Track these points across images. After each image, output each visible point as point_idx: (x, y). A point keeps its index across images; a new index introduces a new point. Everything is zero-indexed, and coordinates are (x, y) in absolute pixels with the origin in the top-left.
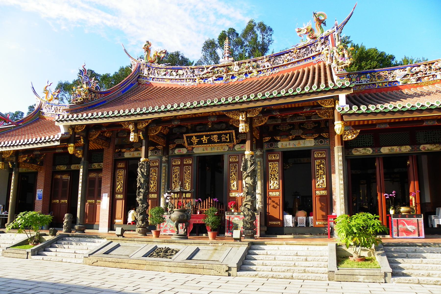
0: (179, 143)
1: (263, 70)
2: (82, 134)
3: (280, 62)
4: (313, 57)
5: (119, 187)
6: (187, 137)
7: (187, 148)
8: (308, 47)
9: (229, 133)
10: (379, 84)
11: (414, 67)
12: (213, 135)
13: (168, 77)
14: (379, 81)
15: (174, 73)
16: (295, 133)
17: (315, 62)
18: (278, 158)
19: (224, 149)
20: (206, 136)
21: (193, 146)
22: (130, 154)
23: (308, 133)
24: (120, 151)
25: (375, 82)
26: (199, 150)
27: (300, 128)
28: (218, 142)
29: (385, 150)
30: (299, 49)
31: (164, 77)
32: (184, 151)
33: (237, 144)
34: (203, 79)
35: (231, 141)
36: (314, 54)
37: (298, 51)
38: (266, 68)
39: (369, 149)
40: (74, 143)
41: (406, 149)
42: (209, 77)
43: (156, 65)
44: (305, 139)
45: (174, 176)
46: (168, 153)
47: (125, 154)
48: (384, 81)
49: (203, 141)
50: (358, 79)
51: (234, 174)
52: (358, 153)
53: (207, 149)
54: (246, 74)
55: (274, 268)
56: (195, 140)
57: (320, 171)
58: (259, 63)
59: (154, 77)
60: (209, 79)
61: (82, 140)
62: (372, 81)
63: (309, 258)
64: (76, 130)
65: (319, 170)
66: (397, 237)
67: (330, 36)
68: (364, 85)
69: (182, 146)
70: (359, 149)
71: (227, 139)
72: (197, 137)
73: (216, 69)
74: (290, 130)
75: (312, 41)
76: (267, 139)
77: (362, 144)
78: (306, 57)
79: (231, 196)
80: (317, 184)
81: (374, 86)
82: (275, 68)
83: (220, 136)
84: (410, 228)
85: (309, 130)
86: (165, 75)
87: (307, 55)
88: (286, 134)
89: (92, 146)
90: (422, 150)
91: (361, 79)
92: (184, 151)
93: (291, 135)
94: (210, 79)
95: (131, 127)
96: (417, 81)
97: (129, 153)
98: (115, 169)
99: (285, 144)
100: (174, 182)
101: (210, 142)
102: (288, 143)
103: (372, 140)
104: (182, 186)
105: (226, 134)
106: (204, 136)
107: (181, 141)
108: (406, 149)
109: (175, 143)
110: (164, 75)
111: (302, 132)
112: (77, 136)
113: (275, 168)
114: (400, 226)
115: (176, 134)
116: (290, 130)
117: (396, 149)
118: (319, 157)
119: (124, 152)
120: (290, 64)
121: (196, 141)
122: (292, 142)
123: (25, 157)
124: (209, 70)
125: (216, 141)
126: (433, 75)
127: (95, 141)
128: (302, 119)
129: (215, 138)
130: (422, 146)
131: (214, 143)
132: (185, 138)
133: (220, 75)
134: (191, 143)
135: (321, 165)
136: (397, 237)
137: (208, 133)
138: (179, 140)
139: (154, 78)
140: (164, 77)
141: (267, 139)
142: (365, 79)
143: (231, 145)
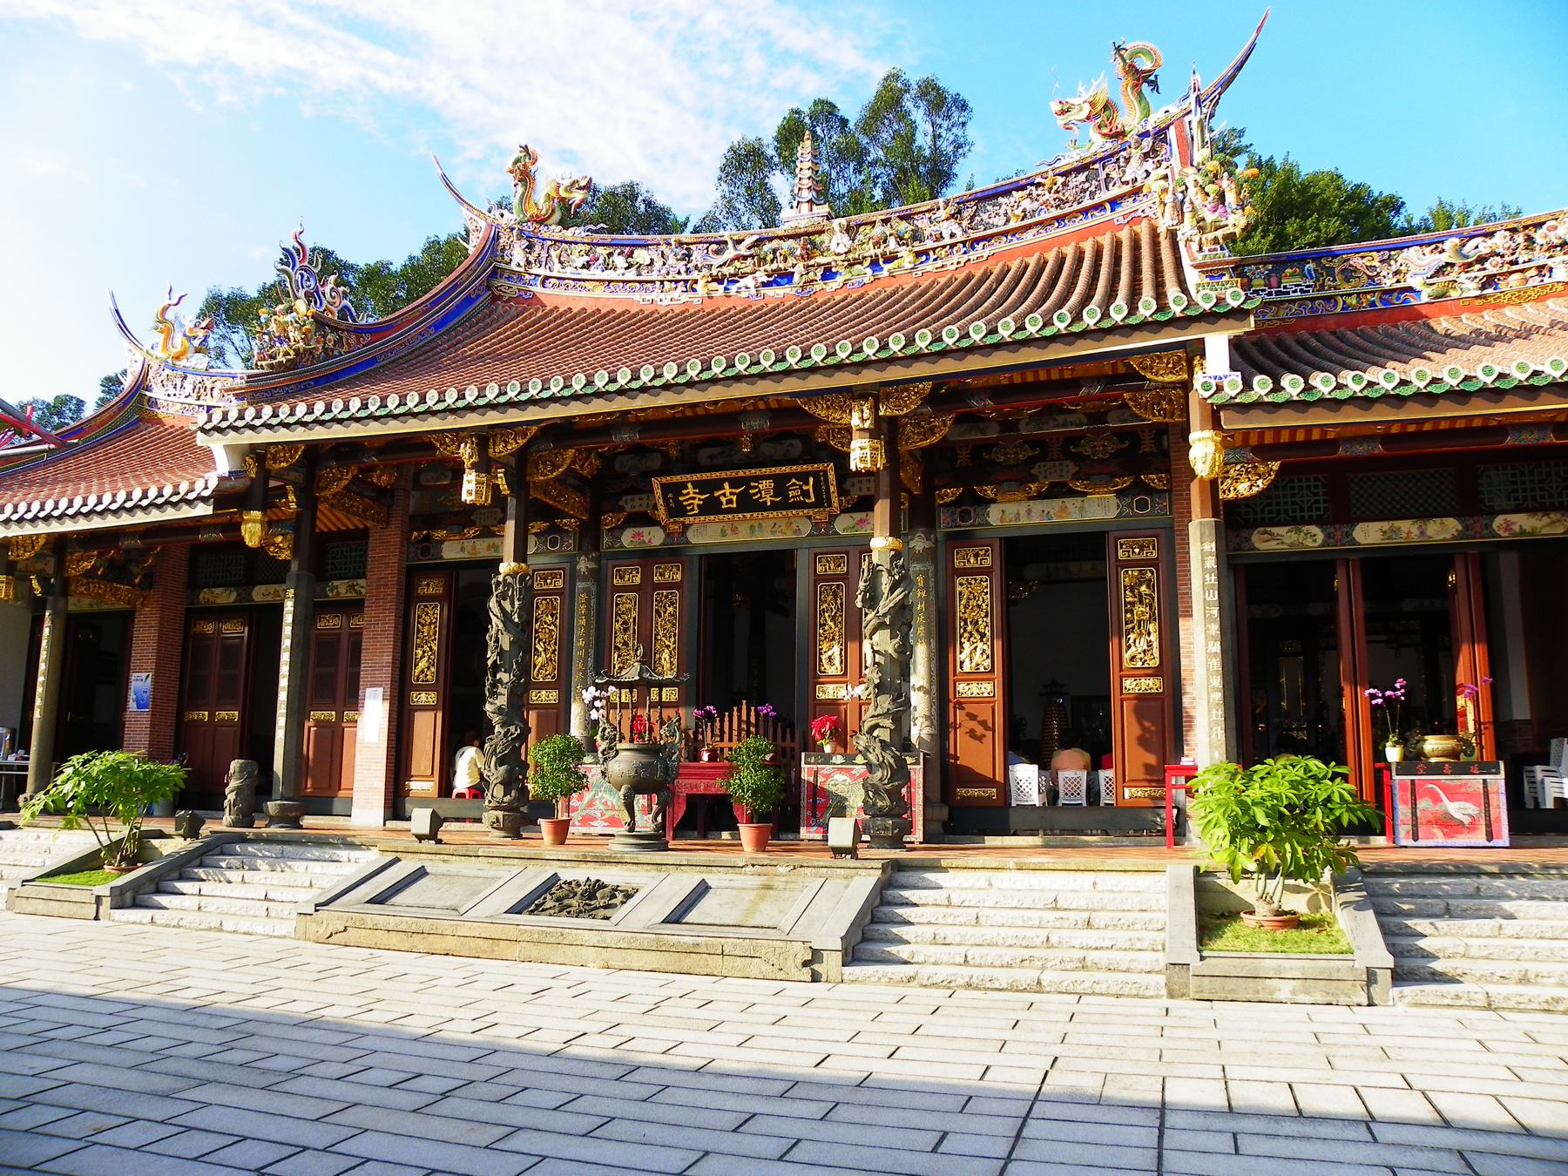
0: (637, 509)
1: (934, 250)
2: (293, 476)
3: (995, 221)
4: (1114, 202)
5: (423, 664)
6: (663, 486)
7: (664, 528)
8: (1097, 166)
9: (815, 474)
10: (1348, 300)
11: (1471, 237)
12: (758, 479)
13: (596, 272)
14: (1346, 288)
15: (620, 261)
16: (1051, 473)
17: (1121, 221)
18: (988, 562)
19: (798, 531)
20: (734, 483)
21: (688, 520)
22: (462, 549)
23: (1094, 473)
24: (427, 538)
25: (1332, 292)
26: (708, 534)
27: (1068, 456)
28: (775, 507)
29: (1368, 534)
30: (1061, 175)
31: (584, 274)
32: (654, 537)
33: (845, 511)
34: (720, 282)
35: (822, 501)
36: (1115, 191)
37: (1060, 180)
38: (948, 241)
39: (1314, 529)
40: (263, 510)
41: (1443, 530)
42: (744, 275)
43: (555, 231)
44: (1084, 494)
45: (617, 626)
46: (596, 546)
47: (445, 546)
48: (1365, 289)
49: (723, 500)
50: (1274, 281)
51: (833, 619)
52: (1272, 546)
53: (734, 531)
54: (874, 264)
55: (974, 953)
56: (693, 497)
57: (1139, 609)
58: (922, 223)
59: (548, 273)
60: (743, 282)
61: (291, 497)
62: (1322, 287)
63: (1099, 919)
64: (270, 464)
65: (1133, 604)
66: (1411, 843)
67: (1172, 128)
68: (1293, 301)
69: (647, 520)
70: (1275, 530)
71: (806, 494)
72: (701, 486)
73: (767, 247)
74: (1030, 461)
75: (1109, 145)
76: (951, 493)
77: (1286, 511)
78: (1087, 203)
79: (821, 696)
80: (1126, 656)
81: (1329, 306)
82: (978, 240)
83: (781, 484)
84: (1458, 809)
85: (1100, 461)
86: (587, 266)
87: (1092, 195)
88: (1017, 478)
89: (329, 519)
90: (1501, 532)
91: (1285, 282)
92: (654, 537)
93: (1034, 479)
94: (748, 281)
95: (466, 452)
96: (1483, 287)
97: (457, 545)
98: (408, 601)
99: (1013, 514)
100: (617, 648)
101: (747, 504)
102: (1022, 508)
103: (1321, 498)
104: (648, 660)
105: (803, 477)
106: (726, 485)
107: (644, 502)
108: (1443, 530)
109: (622, 509)
110: (583, 267)
111: (1072, 468)
112: (272, 483)
113: (978, 598)
114: (1423, 804)
115: (625, 475)
116: (1030, 461)
117: (1408, 531)
118: (1133, 557)
119: (442, 542)
120: (1029, 227)
121: (696, 502)
122: (1038, 506)
123: (88, 559)
124: (743, 249)
125: (768, 500)
126: (1540, 268)
127: (337, 502)
128: (1072, 424)
129: (765, 490)
130: (1499, 521)
131: (762, 507)
132: (658, 492)
133: (782, 266)
134: (678, 510)
135: (1143, 588)
136: (1411, 843)
137: (741, 473)
138: (636, 497)
139: (547, 278)
140: (584, 274)
141: (951, 493)
142: (1298, 280)
143: (820, 515)
